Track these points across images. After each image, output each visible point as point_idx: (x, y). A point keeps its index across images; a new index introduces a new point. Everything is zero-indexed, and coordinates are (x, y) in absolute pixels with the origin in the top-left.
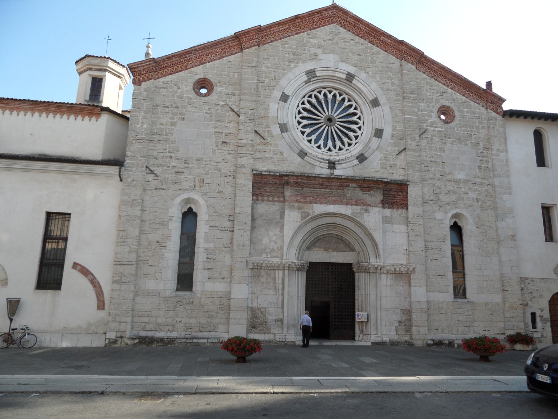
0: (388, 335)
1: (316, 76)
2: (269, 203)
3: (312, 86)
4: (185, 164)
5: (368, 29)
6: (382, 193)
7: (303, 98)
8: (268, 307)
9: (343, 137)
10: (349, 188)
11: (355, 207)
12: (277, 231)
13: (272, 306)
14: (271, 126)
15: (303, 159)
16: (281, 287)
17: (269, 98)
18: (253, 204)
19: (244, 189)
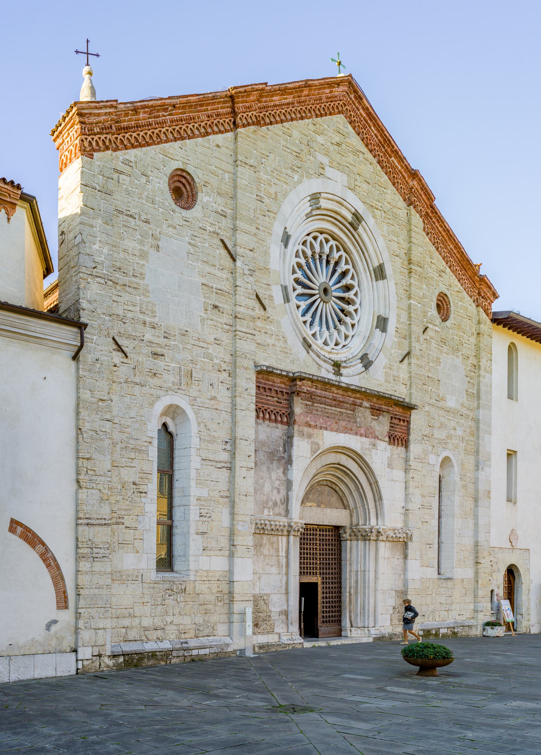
4: (165, 339)
5: (379, 137)
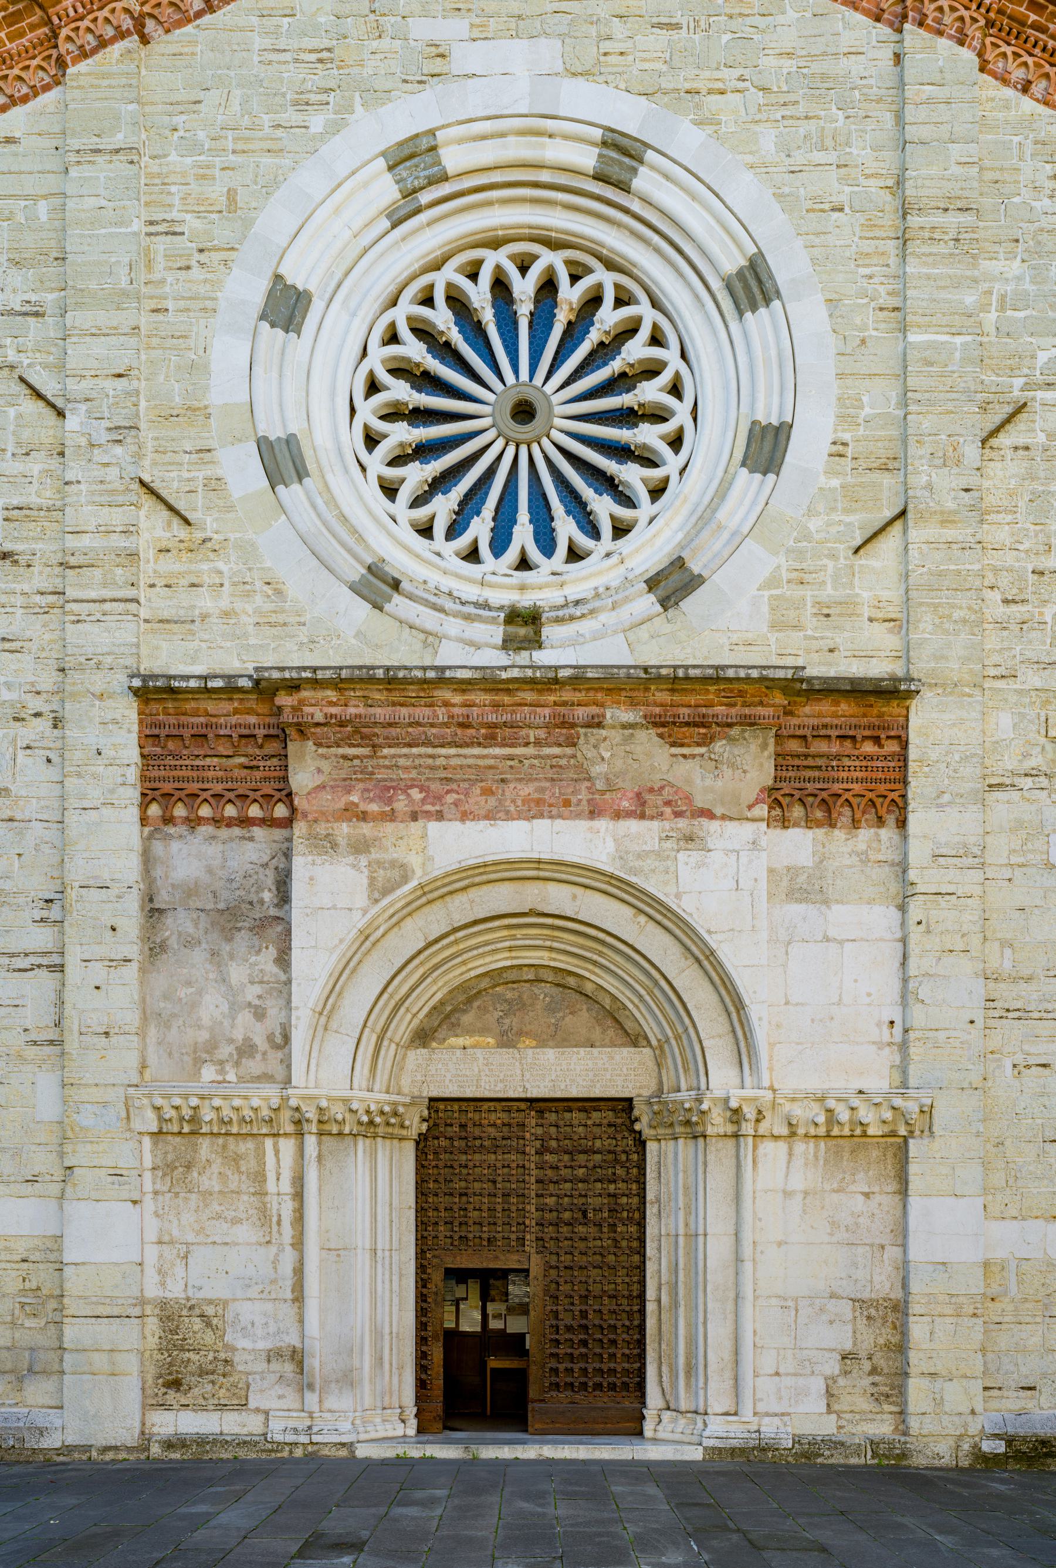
0: (789, 1414)
1: (445, 178)
2: (224, 833)
3: (428, 232)
6: (771, 748)
7: (386, 309)
8: (234, 1300)
9: (587, 492)
10: (604, 733)
11: (633, 826)
12: (268, 956)
13: (254, 1292)
14: (220, 454)
15: (381, 609)
16: (287, 1208)
17: (204, 309)
18: (147, 841)
19: (101, 768)
